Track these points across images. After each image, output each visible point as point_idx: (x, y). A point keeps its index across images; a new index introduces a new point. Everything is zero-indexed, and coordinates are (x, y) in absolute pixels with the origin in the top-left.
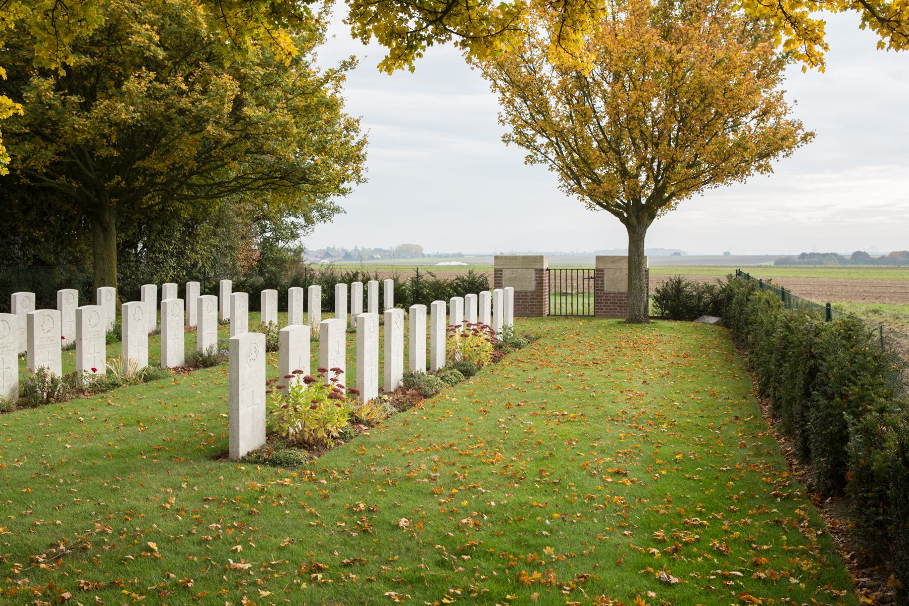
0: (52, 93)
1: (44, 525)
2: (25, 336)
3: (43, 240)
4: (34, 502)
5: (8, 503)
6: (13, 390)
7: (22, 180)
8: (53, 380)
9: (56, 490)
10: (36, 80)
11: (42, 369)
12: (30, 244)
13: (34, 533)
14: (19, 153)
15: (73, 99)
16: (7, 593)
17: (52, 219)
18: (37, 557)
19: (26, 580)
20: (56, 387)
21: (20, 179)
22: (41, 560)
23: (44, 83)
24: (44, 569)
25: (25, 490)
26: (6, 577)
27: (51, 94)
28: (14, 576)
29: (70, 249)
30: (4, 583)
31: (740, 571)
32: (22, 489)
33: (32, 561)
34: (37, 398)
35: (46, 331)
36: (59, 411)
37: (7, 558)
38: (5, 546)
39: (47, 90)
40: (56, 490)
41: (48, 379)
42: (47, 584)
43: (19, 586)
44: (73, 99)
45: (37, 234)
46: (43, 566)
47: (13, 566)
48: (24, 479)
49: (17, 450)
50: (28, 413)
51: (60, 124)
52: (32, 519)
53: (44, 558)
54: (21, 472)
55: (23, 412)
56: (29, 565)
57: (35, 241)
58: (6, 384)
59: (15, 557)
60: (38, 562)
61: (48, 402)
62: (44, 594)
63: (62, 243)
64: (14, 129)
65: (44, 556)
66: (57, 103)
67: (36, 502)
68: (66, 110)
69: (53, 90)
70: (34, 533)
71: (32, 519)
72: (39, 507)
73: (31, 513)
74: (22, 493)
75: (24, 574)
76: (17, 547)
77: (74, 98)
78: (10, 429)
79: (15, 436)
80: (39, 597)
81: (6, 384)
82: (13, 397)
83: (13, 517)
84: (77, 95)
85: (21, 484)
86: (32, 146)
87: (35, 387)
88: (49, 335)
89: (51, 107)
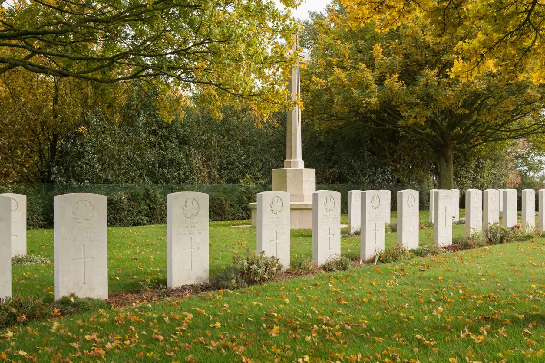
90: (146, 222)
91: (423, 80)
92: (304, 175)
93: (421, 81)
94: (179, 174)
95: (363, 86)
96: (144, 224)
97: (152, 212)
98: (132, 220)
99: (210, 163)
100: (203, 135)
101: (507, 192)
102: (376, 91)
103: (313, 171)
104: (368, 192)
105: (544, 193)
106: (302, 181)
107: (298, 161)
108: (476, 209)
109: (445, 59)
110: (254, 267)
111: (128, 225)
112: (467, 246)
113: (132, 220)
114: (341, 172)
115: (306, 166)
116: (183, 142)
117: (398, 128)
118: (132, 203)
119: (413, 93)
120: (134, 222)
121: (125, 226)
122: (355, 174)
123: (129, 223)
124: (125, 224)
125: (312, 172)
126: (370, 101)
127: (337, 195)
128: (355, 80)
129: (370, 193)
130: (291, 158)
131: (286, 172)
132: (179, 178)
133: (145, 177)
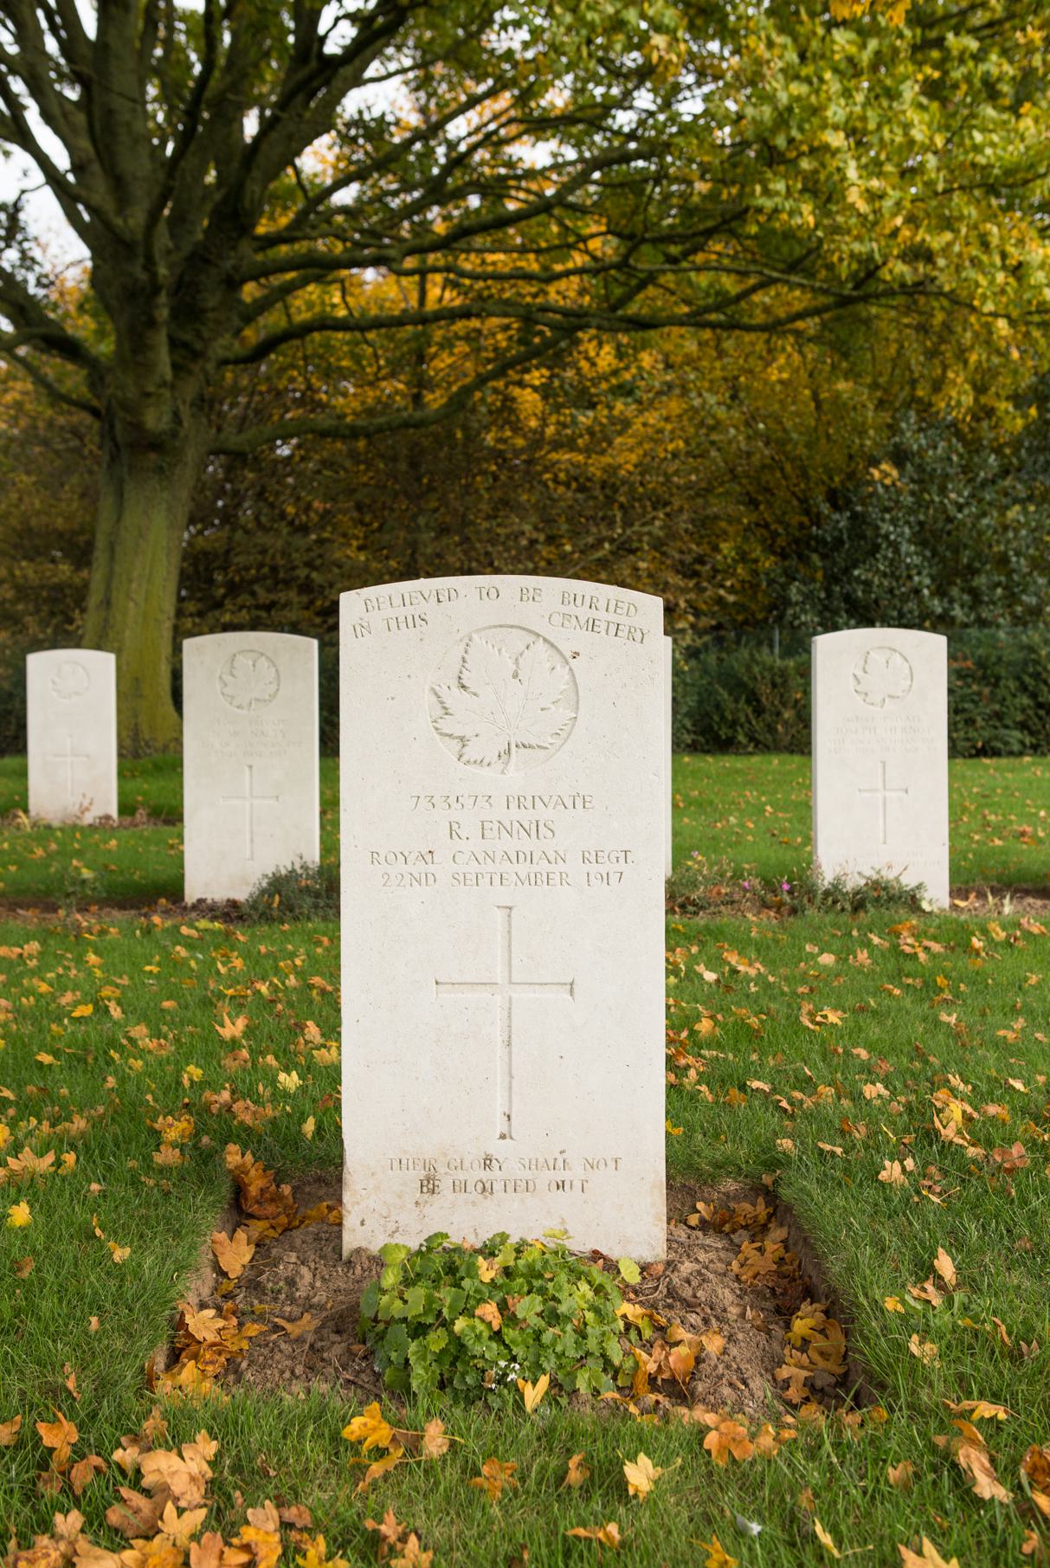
90: (1016, 747)
96: (1011, 754)
98: (968, 739)
113: (968, 739)
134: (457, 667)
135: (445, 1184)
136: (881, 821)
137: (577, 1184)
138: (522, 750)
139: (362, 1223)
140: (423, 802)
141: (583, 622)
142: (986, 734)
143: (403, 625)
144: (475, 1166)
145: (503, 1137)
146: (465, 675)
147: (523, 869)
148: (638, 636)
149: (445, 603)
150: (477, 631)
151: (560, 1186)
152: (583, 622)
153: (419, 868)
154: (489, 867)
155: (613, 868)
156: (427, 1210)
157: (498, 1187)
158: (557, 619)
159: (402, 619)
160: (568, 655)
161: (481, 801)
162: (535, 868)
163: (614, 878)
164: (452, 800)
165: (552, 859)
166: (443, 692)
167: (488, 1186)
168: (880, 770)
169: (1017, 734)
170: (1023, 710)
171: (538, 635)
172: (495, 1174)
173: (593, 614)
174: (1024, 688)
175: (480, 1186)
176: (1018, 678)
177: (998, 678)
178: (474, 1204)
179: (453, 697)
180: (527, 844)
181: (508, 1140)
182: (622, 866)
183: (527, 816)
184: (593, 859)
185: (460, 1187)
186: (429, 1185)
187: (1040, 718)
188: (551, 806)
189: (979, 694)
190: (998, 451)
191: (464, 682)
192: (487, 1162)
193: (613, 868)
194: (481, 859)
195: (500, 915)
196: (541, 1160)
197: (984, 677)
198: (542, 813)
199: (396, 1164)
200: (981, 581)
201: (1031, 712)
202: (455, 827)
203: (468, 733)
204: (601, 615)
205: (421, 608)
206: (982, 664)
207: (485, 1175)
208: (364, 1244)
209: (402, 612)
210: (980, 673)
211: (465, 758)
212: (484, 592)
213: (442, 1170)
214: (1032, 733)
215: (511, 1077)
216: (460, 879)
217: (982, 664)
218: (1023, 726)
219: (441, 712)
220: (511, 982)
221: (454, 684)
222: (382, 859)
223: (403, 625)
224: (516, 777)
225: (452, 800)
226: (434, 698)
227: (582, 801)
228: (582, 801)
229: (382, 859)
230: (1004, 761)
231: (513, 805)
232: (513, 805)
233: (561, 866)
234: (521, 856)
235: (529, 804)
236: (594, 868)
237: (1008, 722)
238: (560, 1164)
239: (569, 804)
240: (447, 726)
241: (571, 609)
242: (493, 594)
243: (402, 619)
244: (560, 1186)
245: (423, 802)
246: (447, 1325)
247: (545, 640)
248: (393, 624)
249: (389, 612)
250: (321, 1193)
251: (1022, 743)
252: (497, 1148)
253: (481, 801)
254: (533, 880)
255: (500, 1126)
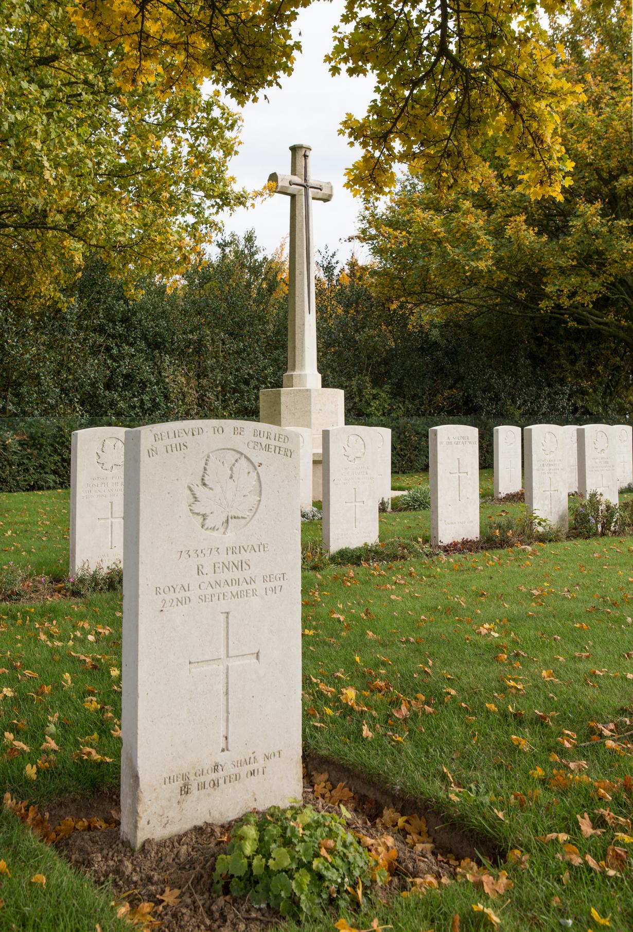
0: (599, 218)
1: (608, 677)
2: (576, 472)
3: (591, 390)
4: (591, 643)
5: (555, 639)
6: (562, 518)
7: (569, 324)
8: (608, 507)
9: (623, 632)
10: (582, 207)
11: (593, 495)
12: (578, 394)
13: (594, 686)
14: (566, 287)
15: (620, 223)
16: (552, 781)
17: (600, 368)
18: (600, 726)
19: (584, 763)
20: (612, 516)
21: (567, 322)
22: (607, 732)
23: (591, 209)
24: (613, 751)
25: (578, 625)
26: (549, 750)
27: (598, 220)
28: (563, 752)
29: (620, 400)
30: (547, 761)
31: (493, 811)
32: (573, 623)
33: (592, 731)
34: (591, 528)
35: (599, 450)
36: (618, 545)
37: (552, 718)
38: (549, 699)
39: (593, 215)
40: (623, 632)
41: (602, 507)
42: (621, 780)
43: (572, 772)
44: (620, 223)
45: (585, 384)
46: (610, 743)
47: (561, 734)
48: (577, 611)
49: (567, 579)
50: (580, 544)
51: (607, 253)
52: (590, 666)
53: (611, 730)
54: (572, 604)
55: (574, 542)
56: (588, 738)
57: (584, 392)
58: (554, 510)
59: (563, 720)
60: (601, 735)
61: (603, 534)
62: (616, 798)
63: (611, 394)
64: (561, 262)
65: (612, 726)
66: (604, 230)
67: (595, 643)
68: (614, 237)
69: (600, 215)
70: (594, 686)
71: (590, 666)
72: (598, 649)
73: (587, 657)
74: (575, 629)
75: (581, 753)
76: (568, 704)
77: (623, 223)
78: (559, 557)
79: (564, 565)
80: (607, 804)
81: (554, 510)
82: (563, 526)
83: (561, 659)
84: (625, 219)
85: (571, 617)
86: (579, 279)
87: (588, 515)
88: (603, 455)
89: (597, 235)
90: (52, 484)
91: (576, 223)
92: (312, 401)
93: (572, 226)
94: (142, 401)
95: (466, 238)
96: (49, 488)
97: (64, 467)
98: (25, 481)
99: (204, 382)
100: (191, 332)
101: (584, 429)
102: (491, 248)
103: (340, 394)
104: (588, 428)
105: (586, 431)
106: (310, 412)
107: (306, 375)
108: (550, 465)
109: (621, 185)
110: (560, 534)
111: (19, 488)
112: (503, 543)
113: (25, 481)
114: (469, 395)
115: (325, 384)
116: (156, 344)
117: (563, 314)
118: (29, 451)
119: (564, 249)
120: (29, 485)
121: (10, 491)
122: (496, 399)
123: (18, 485)
124: (11, 488)
125: (338, 396)
126: (477, 267)
127: (471, 433)
128: (459, 229)
129: (539, 431)
130: (294, 369)
131: (280, 394)
132: (141, 407)
133: (76, 404)
134: (201, 473)
135: (194, 787)
136: (110, 535)
137: (261, 770)
138: (234, 520)
139: (148, 823)
140: (184, 554)
141: (264, 446)
142: (35, 477)
143: (174, 449)
144: (210, 771)
145: (223, 750)
146: (206, 478)
147: (235, 589)
148: (289, 454)
149: (196, 436)
150: (212, 452)
151: (252, 773)
152: (264, 446)
153: (181, 594)
154: (218, 590)
155: (277, 583)
156: (184, 805)
157: (222, 781)
158: (251, 445)
159: (174, 446)
160: (257, 465)
161: (214, 552)
162: (241, 588)
163: (278, 589)
164: (199, 552)
165: (249, 582)
166: (195, 488)
167: (216, 782)
168: (110, 507)
169: (53, 477)
170: (55, 464)
171: (242, 454)
172: (221, 774)
173: (268, 442)
174: (55, 451)
175: (212, 783)
176: (52, 445)
177: (42, 445)
178: (209, 795)
179: (200, 491)
180: (236, 574)
181: (226, 752)
182: (282, 582)
183: (236, 558)
184: (268, 580)
185: (201, 787)
186: (185, 790)
187: (64, 467)
188: (248, 551)
189: (31, 454)
190: (32, 317)
191: (206, 482)
192: (216, 768)
193: (277, 583)
194: (214, 586)
195: (222, 617)
196: (243, 760)
197: (33, 445)
198: (245, 556)
199: (167, 780)
200: (23, 390)
201: (59, 464)
202: (200, 567)
203: (208, 512)
204: (272, 442)
205: (184, 439)
206: (32, 437)
207: (214, 776)
208: (149, 836)
209: (174, 441)
210: (31, 443)
211: (206, 527)
212: (216, 429)
213: (192, 777)
214: (60, 476)
215: (228, 712)
216: (203, 599)
217: (32, 437)
218: (55, 472)
219: (192, 500)
220: (228, 656)
221: (199, 482)
222: (161, 591)
223: (174, 449)
224: (231, 537)
225: (199, 552)
226: (189, 492)
227: (262, 547)
228: (262, 547)
229: (161, 591)
230: (47, 493)
231: (230, 552)
232: (230, 552)
233: (253, 586)
234: (234, 582)
235: (237, 551)
236: (268, 585)
237: (47, 470)
238: (252, 760)
239: (257, 549)
240: (197, 508)
241: (257, 439)
242: (220, 431)
243: (174, 446)
244: (252, 773)
245: (184, 554)
246: (308, 866)
247: (246, 457)
248: (169, 448)
249: (167, 442)
250: (62, 813)
251: (55, 481)
252: (221, 758)
253: (214, 552)
254: (237, 595)
255: (222, 744)
